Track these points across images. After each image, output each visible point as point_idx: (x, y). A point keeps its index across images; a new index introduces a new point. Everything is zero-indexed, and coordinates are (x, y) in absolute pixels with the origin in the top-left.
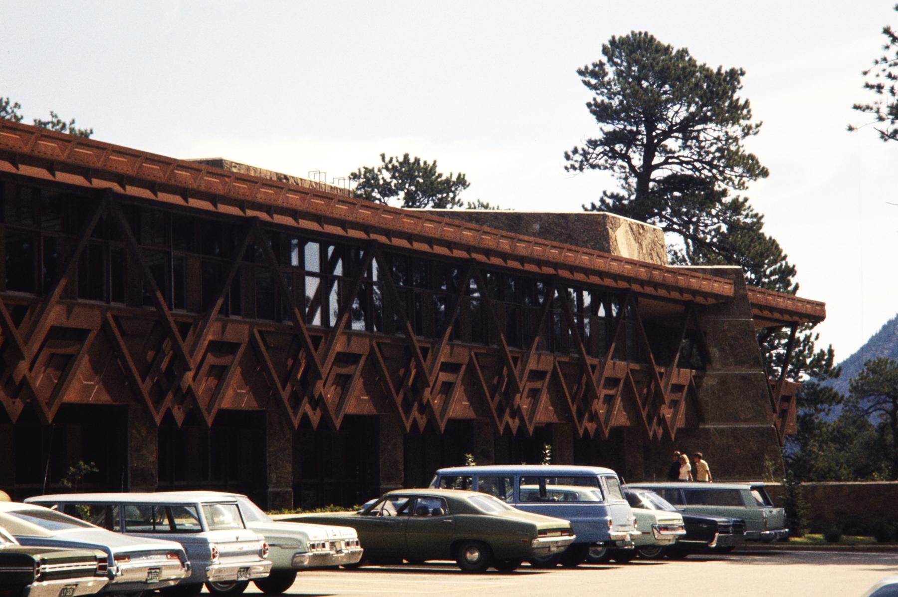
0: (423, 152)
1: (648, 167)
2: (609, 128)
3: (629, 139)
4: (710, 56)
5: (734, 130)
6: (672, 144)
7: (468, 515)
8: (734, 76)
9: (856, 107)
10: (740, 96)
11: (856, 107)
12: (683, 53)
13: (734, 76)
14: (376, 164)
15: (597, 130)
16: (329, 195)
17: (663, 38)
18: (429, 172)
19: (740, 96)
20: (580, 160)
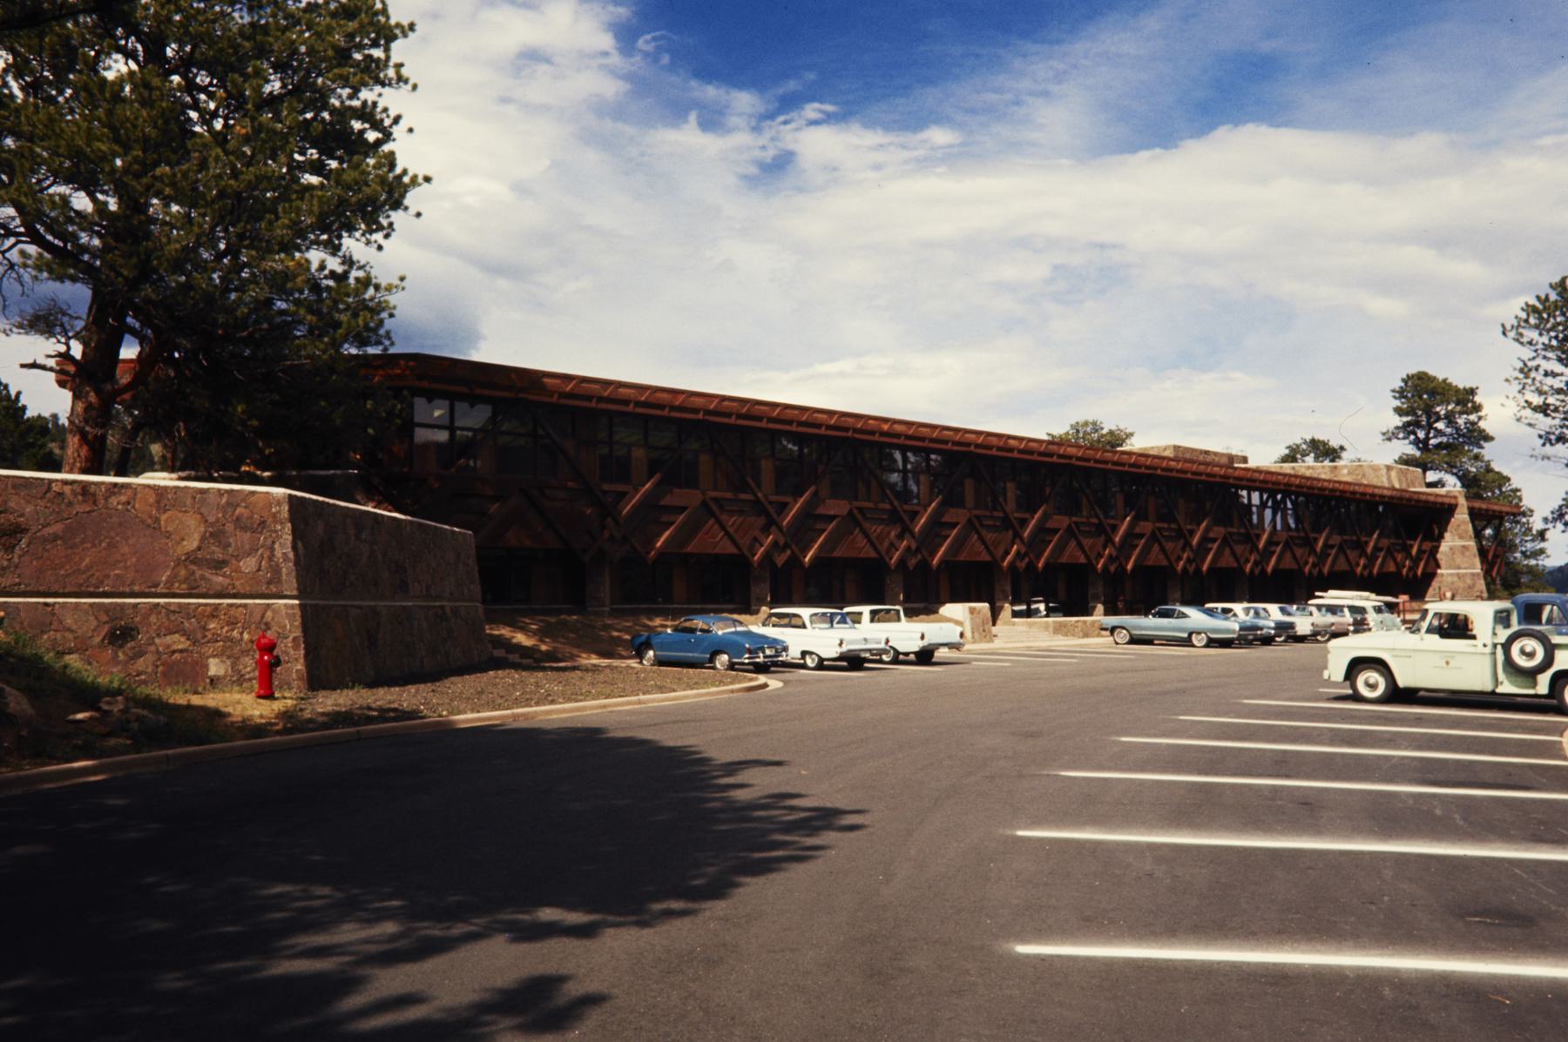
0: (1320, 436)
1: (1427, 438)
2: (1406, 419)
3: (1417, 424)
4: (1460, 381)
5: (1473, 417)
6: (1440, 425)
7: (314, 497)
8: (1472, 392)
9: (23, 366)
10: (1478, 399)
11: (23, 366)
12: (1445, 381)
13: (1472, 392)
14: (1299, 441)
15: (1398, 421)
16: (1040, 442)
17: (1432, 372)
18: (1324, 444)
19: (1478, 399)
20: (1389, 436)
